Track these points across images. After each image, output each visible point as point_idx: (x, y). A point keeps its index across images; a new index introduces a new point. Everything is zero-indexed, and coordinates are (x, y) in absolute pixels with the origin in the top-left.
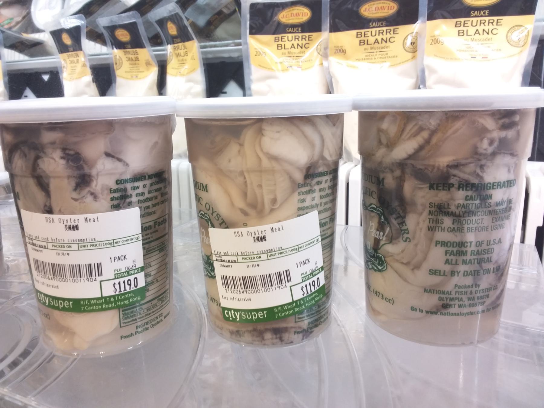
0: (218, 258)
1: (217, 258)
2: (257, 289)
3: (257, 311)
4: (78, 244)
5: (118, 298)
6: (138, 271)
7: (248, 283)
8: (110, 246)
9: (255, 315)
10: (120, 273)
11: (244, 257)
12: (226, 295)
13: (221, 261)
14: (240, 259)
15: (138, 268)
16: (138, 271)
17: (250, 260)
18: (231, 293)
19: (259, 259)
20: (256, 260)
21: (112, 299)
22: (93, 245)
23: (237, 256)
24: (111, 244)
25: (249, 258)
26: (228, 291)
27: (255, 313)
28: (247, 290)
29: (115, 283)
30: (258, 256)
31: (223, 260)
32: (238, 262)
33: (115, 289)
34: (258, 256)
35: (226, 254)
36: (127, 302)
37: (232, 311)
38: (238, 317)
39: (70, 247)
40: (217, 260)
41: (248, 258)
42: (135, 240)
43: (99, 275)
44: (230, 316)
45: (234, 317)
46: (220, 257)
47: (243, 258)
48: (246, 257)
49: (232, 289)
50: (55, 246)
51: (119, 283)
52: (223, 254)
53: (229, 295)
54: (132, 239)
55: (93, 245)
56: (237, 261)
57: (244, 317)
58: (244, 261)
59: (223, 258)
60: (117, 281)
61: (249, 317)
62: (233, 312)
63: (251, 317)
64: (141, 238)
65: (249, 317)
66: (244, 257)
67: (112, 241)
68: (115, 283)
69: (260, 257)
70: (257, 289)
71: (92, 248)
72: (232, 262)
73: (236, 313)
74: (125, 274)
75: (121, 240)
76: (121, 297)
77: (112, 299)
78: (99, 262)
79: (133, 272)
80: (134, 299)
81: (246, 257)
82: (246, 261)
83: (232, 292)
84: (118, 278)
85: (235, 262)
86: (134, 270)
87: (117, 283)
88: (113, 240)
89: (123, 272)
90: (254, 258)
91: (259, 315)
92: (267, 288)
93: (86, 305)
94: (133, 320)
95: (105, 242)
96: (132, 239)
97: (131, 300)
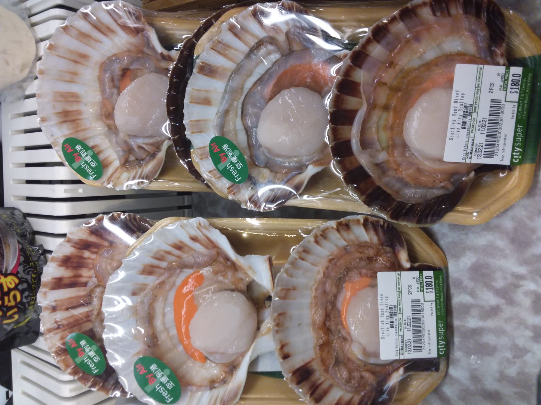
0: (469, 157)
1: (469, 158)
2: (498, 128)
3: (516, 132)
4: (398, 313)
5: (437, 291)
6: (421, 276)
7: (492, 133)
8: (401, 294)
9: (519, 135)
10: (420, 288)
11: (471, 131)
12: (500, 157)
13: (471, 153)
14: (472, 135)
15: (420, 275)
16: (421, 276)
17: (475, 127)
18: (498, 150)
19: (475, 120)
20: (475, 122)
21: (438, 295)
22: (400, 304)
23: (469, 137)
24: (399, 293)
25: (473, 127)
26: (497, 154)
27: (517, 134)
28: (498, 136)
29: (426, 292)
30: (472, 120)
31: (470, 151)
32: (474, 137)
33: (430, 292)
34: (472, 120)
35: (466, 149)
36: (441, 285)
37: (513, 154)
38: (519, 149)
39: (400, 319)
40: (471, 158)
41: (473, 128)
42: (400, 277)
43: (420, 302)
44: (518, 157)
45: (519, 154)
46: (468, 154)
47: (472, 132)
48: (471, 130)
49: (496, 148)
50: (401, 329)
51: (427, 289)
52: (466, 151)
53: (500, 153)
54: (399, 279)
55: (400, 304)
56: (473, 138)
57: (519, 144)
58: (474, 132)
59: (469, 151)
60: (425, 291)
61: (519, 140)
62: (514, 154)
63: (520, 139)
64: (399, 272)
65: (519, 140)
66: (471, 131)
67: (398, 292)
68: (426, 292)
69: (474, 119)
70: (498, 128)
71: (401, 305)
72: (473, 143)
73: (515, 151)
74: (422, 285)
75: (398, 286)
76: (437, 289)
77: (438, 295)
78: (411, 301)
79: (421, 279)
80: (441, 280)
81: (471, 130)
82: (474, 131)
83: (498, 149)
84: (423, 290)
85: (473, 140)
86: (420, 278)
87: (426, 290)
88: (397, 291)
89: (420, 286)
90: (473, 123)
91: (519, 131)
92: (500, 120)
93: (440, 312)
94: (439, 290)
95: (398, 297)
96: (399, 279)
97: (441, 282)
